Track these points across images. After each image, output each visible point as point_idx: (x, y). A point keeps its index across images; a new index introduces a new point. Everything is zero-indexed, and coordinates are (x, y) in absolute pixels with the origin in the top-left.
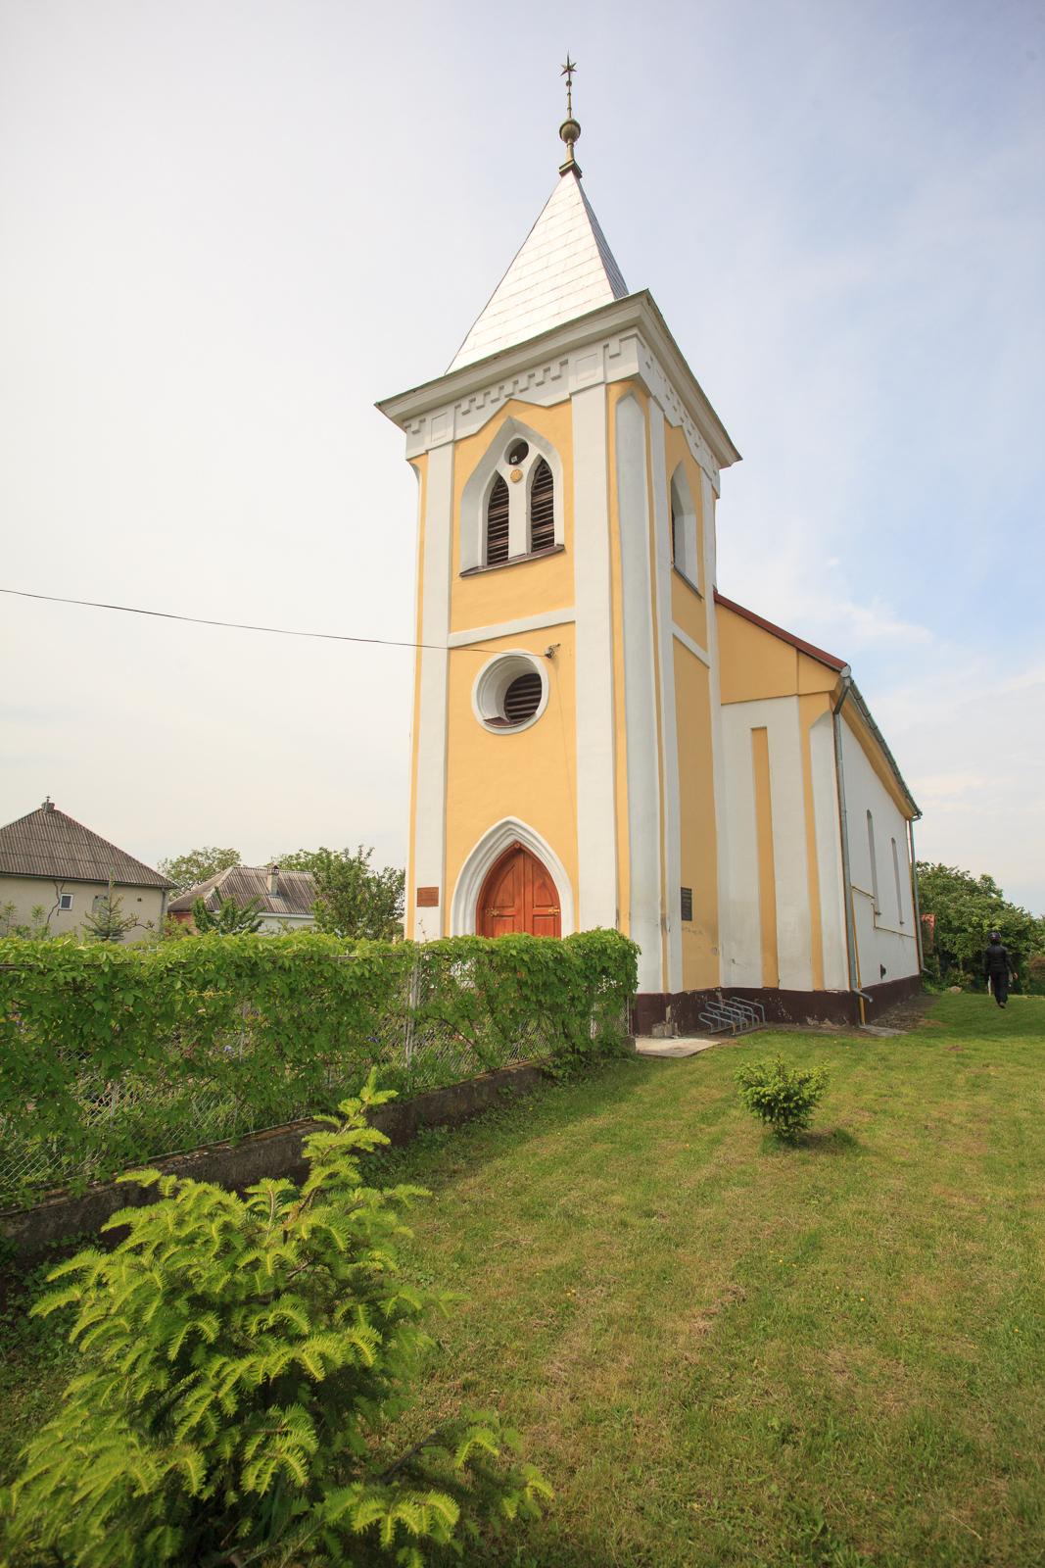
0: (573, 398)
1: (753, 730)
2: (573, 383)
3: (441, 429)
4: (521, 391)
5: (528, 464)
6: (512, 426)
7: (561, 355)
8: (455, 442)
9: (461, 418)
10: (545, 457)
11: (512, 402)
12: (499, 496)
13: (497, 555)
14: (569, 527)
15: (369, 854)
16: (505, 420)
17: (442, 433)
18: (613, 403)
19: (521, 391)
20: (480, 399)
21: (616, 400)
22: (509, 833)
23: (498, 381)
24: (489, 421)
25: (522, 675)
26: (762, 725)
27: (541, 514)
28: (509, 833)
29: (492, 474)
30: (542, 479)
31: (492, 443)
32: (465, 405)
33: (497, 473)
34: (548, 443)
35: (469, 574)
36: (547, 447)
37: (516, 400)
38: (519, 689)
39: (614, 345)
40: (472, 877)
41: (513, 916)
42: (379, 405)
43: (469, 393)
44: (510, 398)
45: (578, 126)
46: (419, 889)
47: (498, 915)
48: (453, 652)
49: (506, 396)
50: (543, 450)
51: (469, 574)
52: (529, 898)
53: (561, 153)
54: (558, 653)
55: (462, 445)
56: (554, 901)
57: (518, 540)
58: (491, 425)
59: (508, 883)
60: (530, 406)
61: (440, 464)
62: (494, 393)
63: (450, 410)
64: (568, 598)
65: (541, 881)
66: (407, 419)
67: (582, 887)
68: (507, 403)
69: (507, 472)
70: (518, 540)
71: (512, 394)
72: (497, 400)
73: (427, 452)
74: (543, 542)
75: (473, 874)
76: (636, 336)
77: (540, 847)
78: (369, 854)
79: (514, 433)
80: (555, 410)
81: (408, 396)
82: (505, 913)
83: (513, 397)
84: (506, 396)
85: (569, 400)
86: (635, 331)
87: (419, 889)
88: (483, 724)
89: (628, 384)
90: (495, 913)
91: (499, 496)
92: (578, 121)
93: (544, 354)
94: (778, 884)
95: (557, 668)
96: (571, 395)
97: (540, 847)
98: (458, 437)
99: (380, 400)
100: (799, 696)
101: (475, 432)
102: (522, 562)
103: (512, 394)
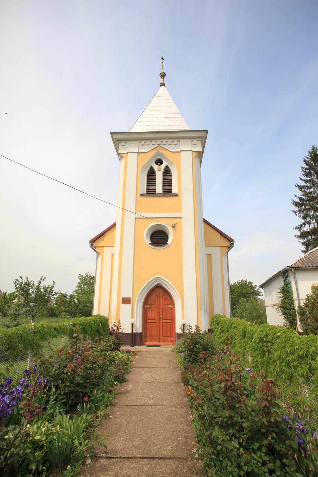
0: (181, 152)
1: (207, 254)
2: (182, 148)
3: (132, 148)
4: (163, 145)
5: (163, 166)
6: (158, 154)
7: (179, 139)
8: (138, 153)
9: (141, 146)
10: (169, 166)
11: (159, 147)
12: (151, 173)
13: (151, 191)
14: (179, 188)
15: (44, 280)
16: (156, 151)
17: (134, 149)
18: (194, 157)
19: (163, 145)
20: (148, 143)
21: (194, 157)
22: (157, 281)
23: (156, 139)
24: (151, 150)
25: (166, 232)
26: (210, 254)
27: (167, 182)
28: (157, 281)
29: (150, 166)
30: (167, 172)
31: (152, 157)
32: (143, 143)
33: (152, 166)
34: (172, 162)
35: (142, 195)
36: (171, 163)
37: (161, 147)
38: (155, 234)
39: (195, 141)
40: (143, 294)
41: (155, 308)
42: (112, 133)
43: (145, 140)
44: (159, 145)
45: (165, 75)
46: (122, 298)
47: (149, 308)
48: (137, 220)
49: (158, 144)
50: (169, 164)
51: (142, 195)
52: (161, 302)
53: (161, 80)
54: (176, 226)
55: (141, 155)
56: (173, 304)
57: (159, 188)
58: (152, 151)
59: (153, 296)
60: (165, 150)
61: (132, 159)
62: (154, 142)
63: (137, 142)
64: (180, 210)
65: (166, 297)
66: (120, 141)
67: (185, 299)
68: (157, 147)
69: (156, 167)
70: (159, 188)
71: (160, 144)
72: (155, 145)
73: (127, 153)
74: (167, 191)
75: (143, 293)
76: (201, 141)
77: (169, 286)
78: (44, 280)
79: (158, 156)
80: (175, 154)
81: (124, 134)
82: (152, 307)
83: (160, 145)
84: (158, 144)
85: (180, 152)
86: (201, 140)
87: (122, 298)
88: (149, 245)
89: (198, 153)
90: (148, 306)
91: (151, 173)
92: (166, 74)
93: (174, 136)
94: (214, 299)
95: (176, 231)
96: (181, 151)
97: (169, 286)
98: (140, 152)
99: (112, 132)
100: (220, 246)
101: (146, 152)
102: (159, 195)
103: (160, 144)
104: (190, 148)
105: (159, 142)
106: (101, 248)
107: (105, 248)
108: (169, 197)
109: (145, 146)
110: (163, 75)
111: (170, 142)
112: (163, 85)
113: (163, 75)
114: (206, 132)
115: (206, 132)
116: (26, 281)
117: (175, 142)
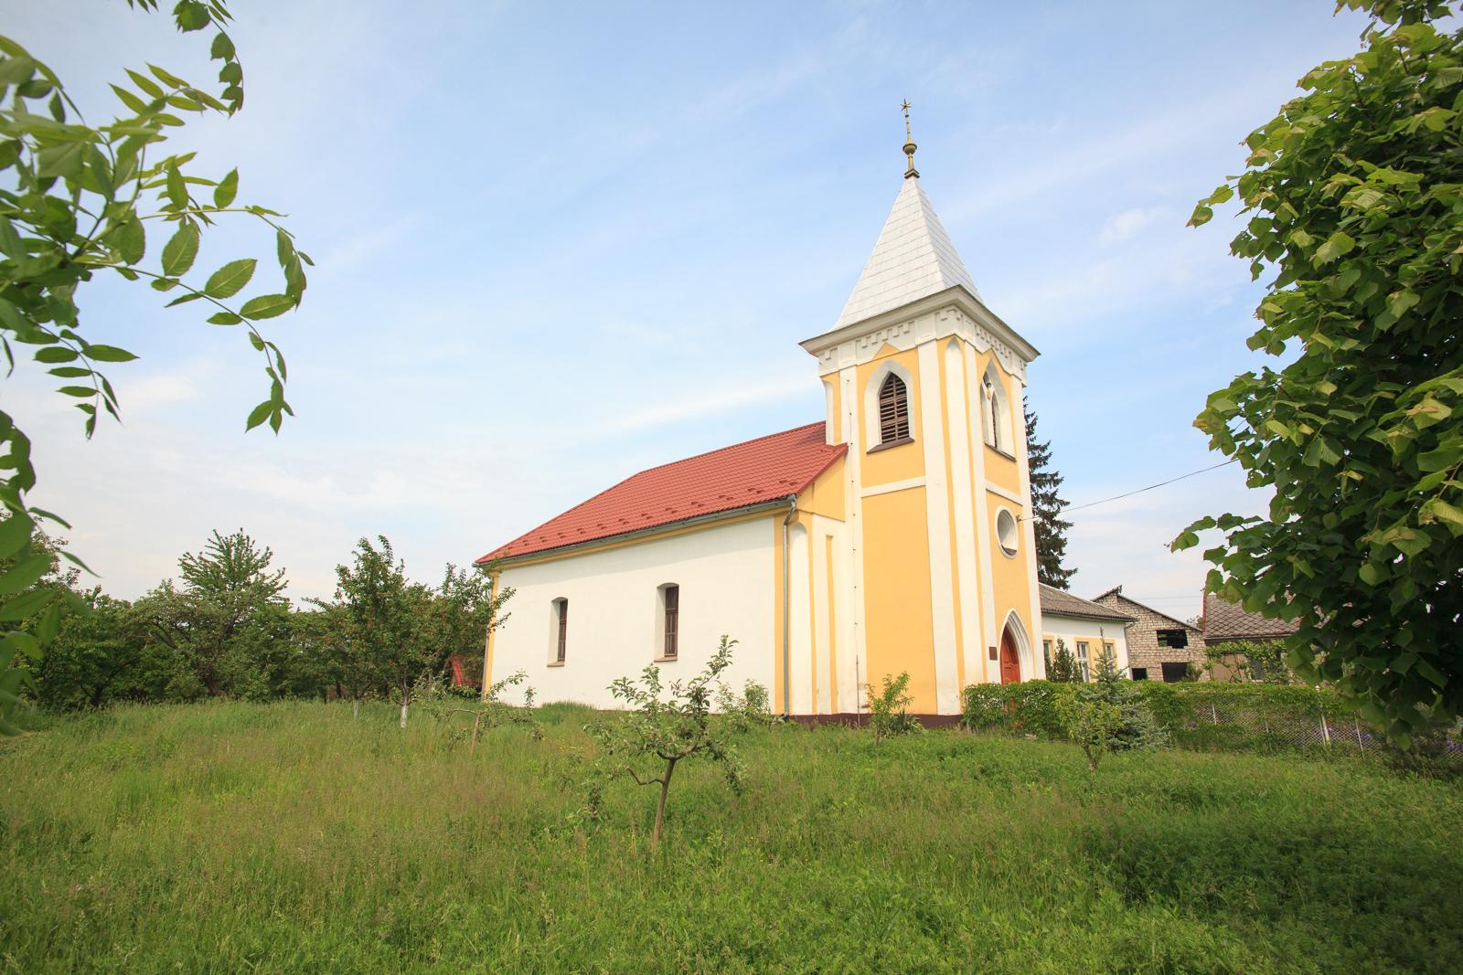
32: (864, 341)
39: (943, 314)
46: (990, 648)
53: (903, 163)
72: (876, 343)
87: (990, 648)
104: (934, 335)
105: (884, 334)
106: (808, 516)
107: (815, 516)
108: (649, 546)
109: (870, 347)
110: (909, 150)
111: (895, 331)
112: (912, 174)
113: (909, 150)
114: (824, 423)
115: (824, 423)
116: (769, 682)
117: (906, 327)
